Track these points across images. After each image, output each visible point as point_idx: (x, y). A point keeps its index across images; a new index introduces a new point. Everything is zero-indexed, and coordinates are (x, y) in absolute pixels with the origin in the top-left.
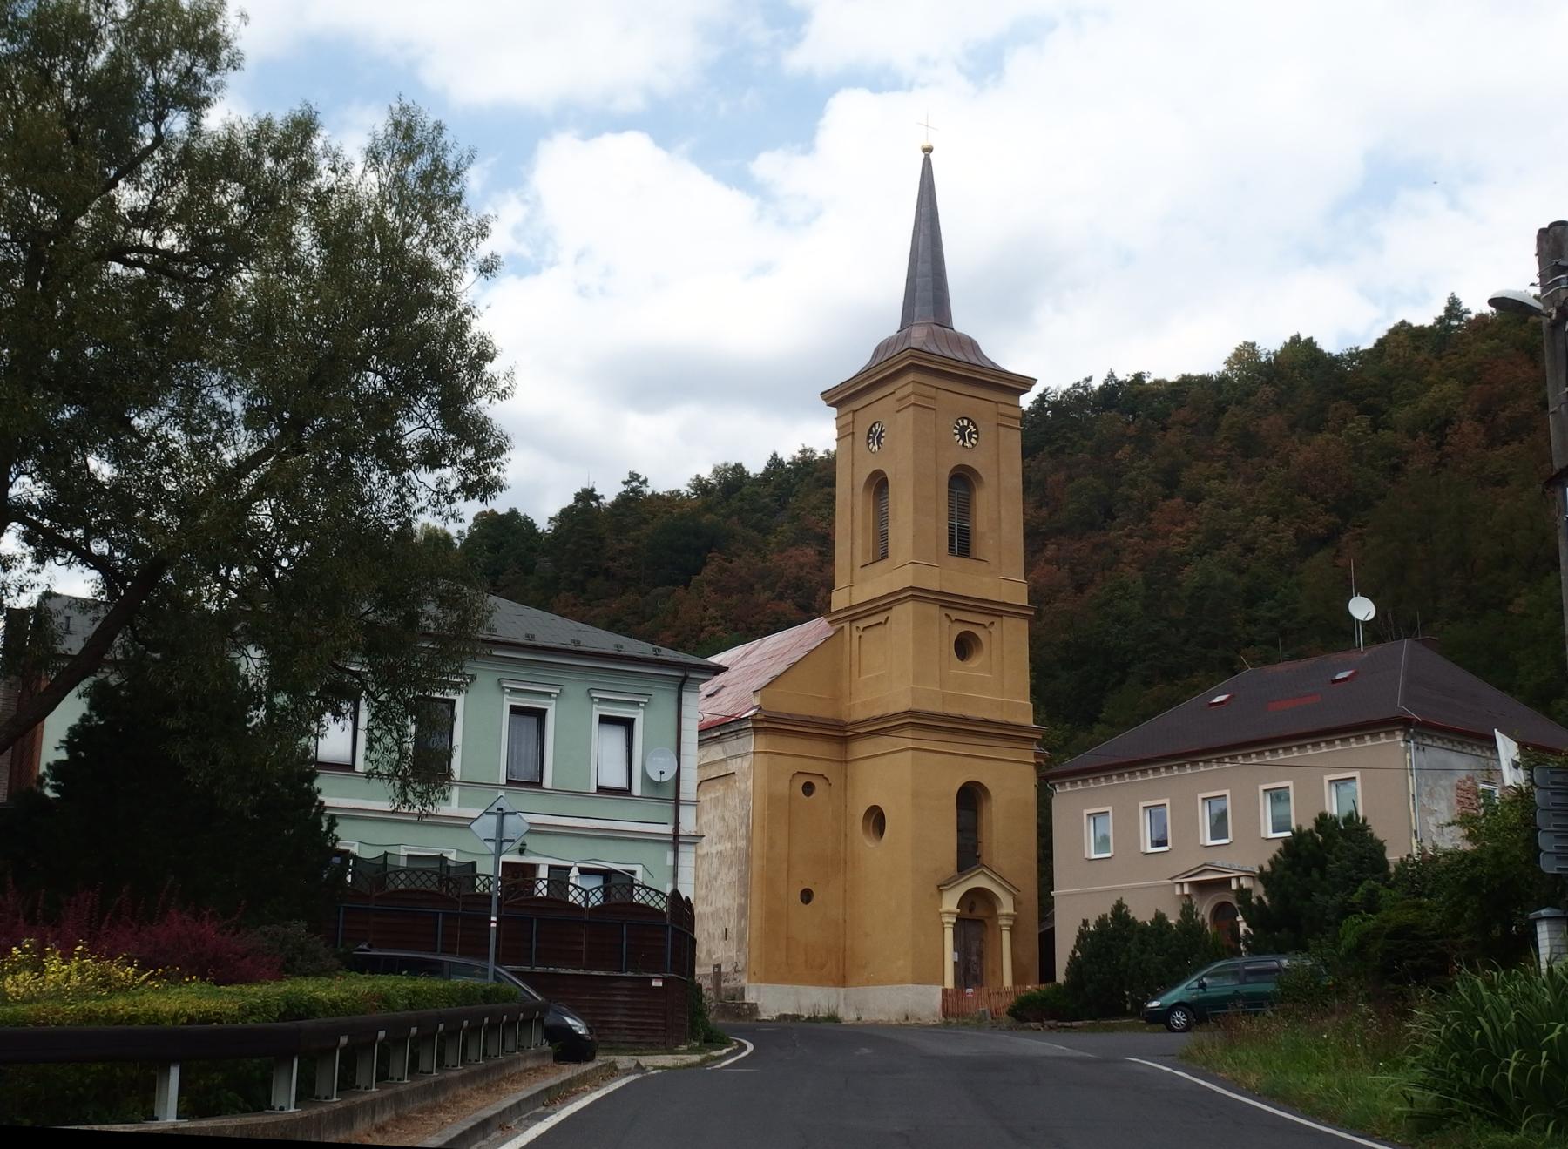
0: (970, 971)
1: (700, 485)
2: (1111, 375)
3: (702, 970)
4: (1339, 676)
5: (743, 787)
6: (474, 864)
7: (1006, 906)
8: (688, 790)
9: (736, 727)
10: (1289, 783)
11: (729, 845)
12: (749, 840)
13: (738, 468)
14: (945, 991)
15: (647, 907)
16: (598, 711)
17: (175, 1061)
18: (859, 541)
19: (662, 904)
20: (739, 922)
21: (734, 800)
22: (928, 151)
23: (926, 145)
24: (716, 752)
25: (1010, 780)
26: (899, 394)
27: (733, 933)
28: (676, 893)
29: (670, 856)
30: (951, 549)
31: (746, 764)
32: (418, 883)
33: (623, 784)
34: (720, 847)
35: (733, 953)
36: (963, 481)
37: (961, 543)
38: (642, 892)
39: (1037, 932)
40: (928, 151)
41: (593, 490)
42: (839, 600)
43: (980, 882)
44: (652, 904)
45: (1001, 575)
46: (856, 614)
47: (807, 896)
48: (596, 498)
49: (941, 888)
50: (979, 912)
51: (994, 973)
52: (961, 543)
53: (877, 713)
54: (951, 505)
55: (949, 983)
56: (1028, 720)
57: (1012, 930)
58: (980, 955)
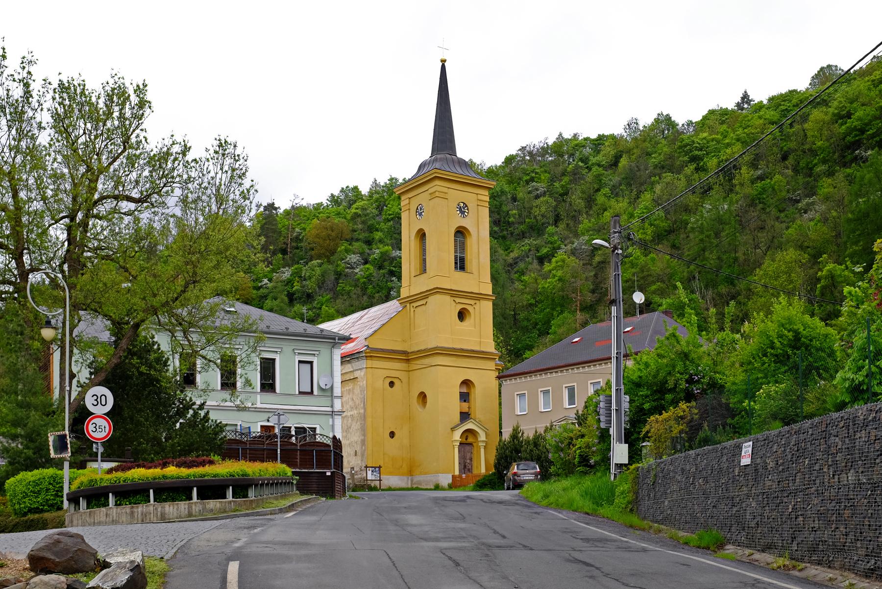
0: (465, 466)
1: (334, 199)
2: (560, 135)
3: (346, 470)
7: (482, 437)
8: (337, 391)
9: (357, 356)
10: (575, 384)
13: (356, 188)
14: (453, 476)
21: (357, 391)
22: (443, 61)
23: (444, 58)
24: (348, 368)
25: (485, 378)
26: (431, 191)
27: (359, 453)
28: (334, 437)
29: (331, 420)
30: (456, 268)
31: (362, 374)
34: (352, 413)
35: (359, 462)
36: (461, 233)
37: (461, 264)
40: (443, 61)
41: (273, 204)
42: (404, 293)
43: (469, 425)
45: (479, 278)
46: (412, 300)
47: (392, 435)
48: (276, 209)
49: (453, 429)
50: (470, 440)
52: (461, 264)
53: (423, 348)
54: (455, 246)
55: (457, 473)
56: (493, 350)
58: (471, 459)
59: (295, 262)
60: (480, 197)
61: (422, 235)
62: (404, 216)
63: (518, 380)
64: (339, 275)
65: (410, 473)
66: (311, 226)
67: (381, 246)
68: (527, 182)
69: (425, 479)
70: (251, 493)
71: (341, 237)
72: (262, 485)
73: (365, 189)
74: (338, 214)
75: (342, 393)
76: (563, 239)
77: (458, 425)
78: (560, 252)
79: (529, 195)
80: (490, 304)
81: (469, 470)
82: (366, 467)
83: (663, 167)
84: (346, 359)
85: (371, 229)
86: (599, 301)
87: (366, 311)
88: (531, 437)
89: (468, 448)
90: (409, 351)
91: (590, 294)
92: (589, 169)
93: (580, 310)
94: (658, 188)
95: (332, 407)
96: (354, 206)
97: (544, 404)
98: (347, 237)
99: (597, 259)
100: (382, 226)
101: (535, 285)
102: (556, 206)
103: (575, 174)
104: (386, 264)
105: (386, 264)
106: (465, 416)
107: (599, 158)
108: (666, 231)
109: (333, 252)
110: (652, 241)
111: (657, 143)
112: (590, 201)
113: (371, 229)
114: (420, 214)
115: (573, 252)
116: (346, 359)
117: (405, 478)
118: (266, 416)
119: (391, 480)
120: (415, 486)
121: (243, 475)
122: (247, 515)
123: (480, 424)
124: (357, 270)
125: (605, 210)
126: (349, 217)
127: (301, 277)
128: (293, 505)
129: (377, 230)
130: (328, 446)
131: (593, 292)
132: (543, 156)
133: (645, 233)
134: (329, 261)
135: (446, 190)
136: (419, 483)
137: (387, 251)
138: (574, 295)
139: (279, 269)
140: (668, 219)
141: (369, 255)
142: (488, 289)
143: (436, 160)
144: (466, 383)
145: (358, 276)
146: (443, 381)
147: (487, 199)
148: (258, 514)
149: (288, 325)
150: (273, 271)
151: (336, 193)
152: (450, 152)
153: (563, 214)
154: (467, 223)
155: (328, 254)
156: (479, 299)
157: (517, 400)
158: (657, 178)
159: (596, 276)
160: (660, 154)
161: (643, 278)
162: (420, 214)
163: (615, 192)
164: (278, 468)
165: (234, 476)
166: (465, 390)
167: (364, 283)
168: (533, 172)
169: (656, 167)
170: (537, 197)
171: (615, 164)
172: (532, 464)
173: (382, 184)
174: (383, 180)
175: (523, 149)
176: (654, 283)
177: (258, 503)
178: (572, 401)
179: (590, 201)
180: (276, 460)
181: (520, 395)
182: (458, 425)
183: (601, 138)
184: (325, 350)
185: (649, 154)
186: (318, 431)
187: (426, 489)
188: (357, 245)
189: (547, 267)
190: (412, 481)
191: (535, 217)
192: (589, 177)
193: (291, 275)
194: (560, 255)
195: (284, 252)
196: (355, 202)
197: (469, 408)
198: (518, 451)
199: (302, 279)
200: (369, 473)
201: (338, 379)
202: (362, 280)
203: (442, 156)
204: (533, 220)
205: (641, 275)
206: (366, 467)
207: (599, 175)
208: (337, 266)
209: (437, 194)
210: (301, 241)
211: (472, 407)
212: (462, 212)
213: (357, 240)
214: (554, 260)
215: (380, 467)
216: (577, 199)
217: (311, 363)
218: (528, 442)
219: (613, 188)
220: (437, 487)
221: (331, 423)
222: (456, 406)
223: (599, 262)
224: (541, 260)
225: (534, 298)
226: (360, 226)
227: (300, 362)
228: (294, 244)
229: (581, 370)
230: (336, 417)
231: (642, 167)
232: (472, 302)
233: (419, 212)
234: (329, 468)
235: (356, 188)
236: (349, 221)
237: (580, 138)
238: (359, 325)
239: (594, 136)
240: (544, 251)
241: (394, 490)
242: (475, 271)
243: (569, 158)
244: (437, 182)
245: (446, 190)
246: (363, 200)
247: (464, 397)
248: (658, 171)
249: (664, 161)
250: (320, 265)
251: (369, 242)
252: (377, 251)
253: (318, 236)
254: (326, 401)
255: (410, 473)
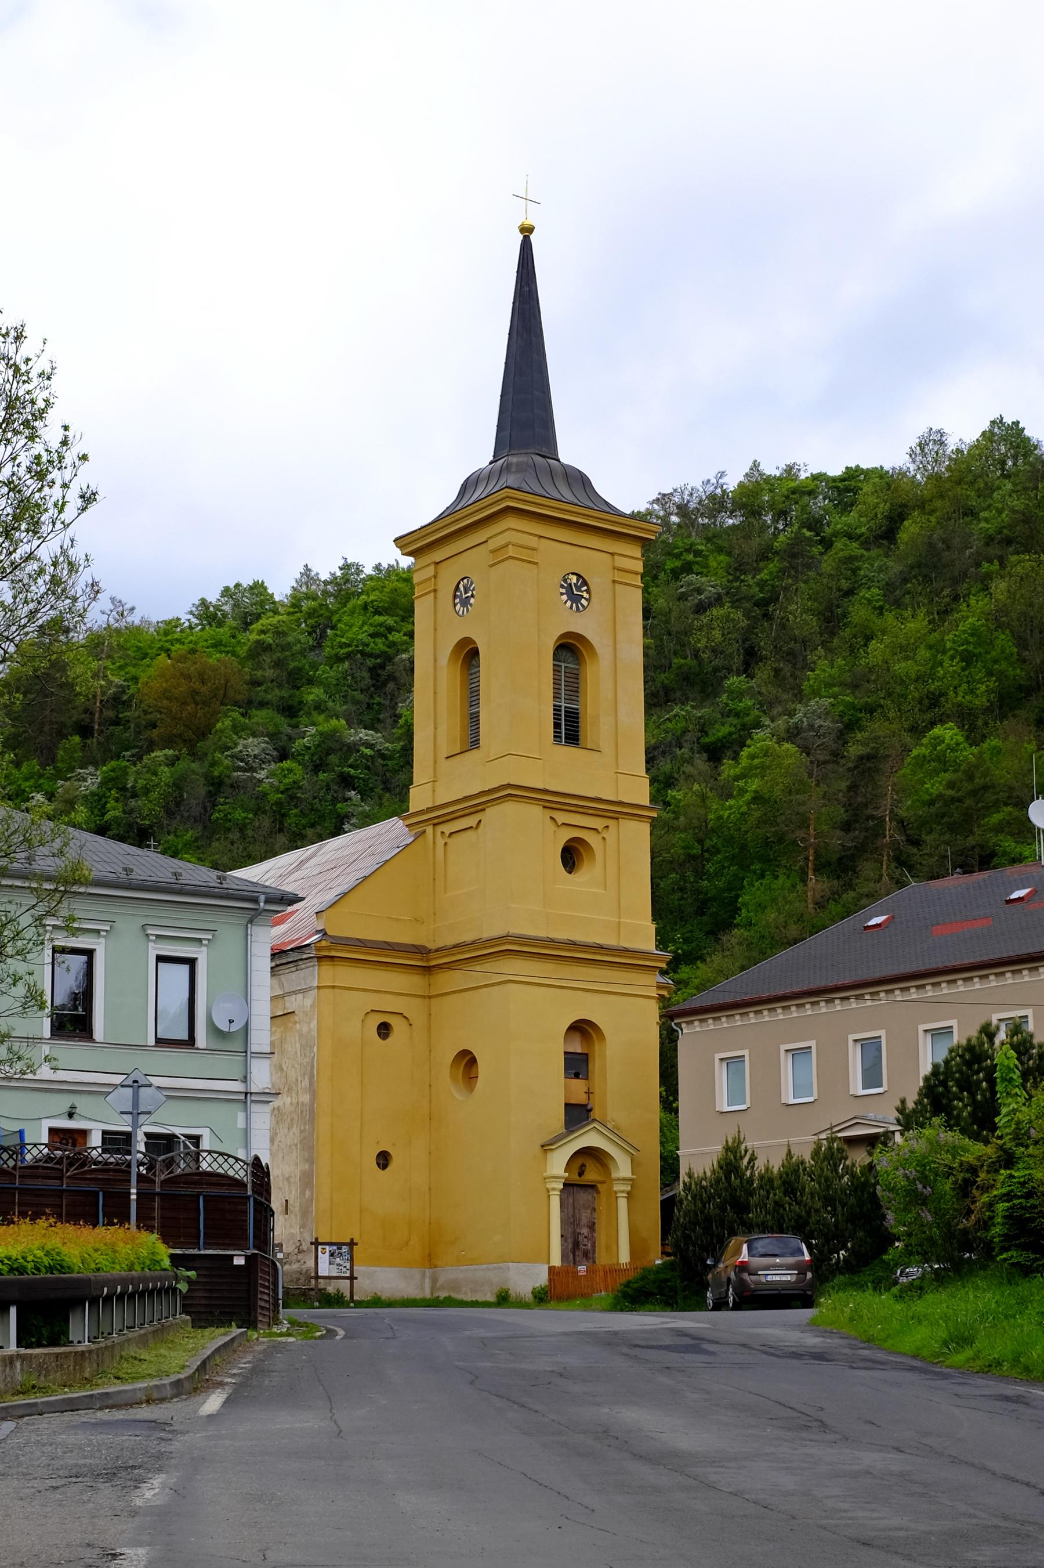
0: (578, 1244)
1: (207, 614)
2: (755, 465)
4: (1015, 895)
5: (305, 1029)
6: (21, 1133)
7: (623, 1168)
8: (261, 1038)
11: (288, 1100)
12: (313, 1091)
13: (258, 588)
14: (551, 1269)
15: (225, 1176)
16: (155, 950)
17: (13, 1304)
18: (443, 728)
19: (242, 1173)
20: (303, 1193)
22: (527, 231)
23: (529, 222)
26: (493, 544)
29: (241, 1116)
30: (557, 737)
31: (308, 1002)
32: (226, 1166)
33: (184, 1036)
35: (296, 1230)
36: (570, 650)
37: (569, 728)
38: (209, 1159)
39: (659, 1198)
40: (527, 231)
42: (419, 798)
43: (589, 1138)
44: (231, 1173)
45: (617, 760)
46: (440, 816)
47: (384, 1159)
49: (547, 1147)
50: (591, 1175)
51: (608, 1248)
52: (569, 728)
53: (468, 938)
54: (556, 682)
55: (556, 1261)
57: (630, 1196)
58: (592, 1227)
59: (109, 754)
60: (621, 562)
61: (469, 655)
62: (422, 609)
63: (724, 1023)
64: (217, 786)
65: (430, 1260)
66: (151, 671)
67: (321, 718)
68: (676, 574)
69: (477, 1279)
70: (80, 1330)
71: (223, 696)
72: (108, 1299)
73: (281, 589)
74: (217, 645)
75: (272, 1044)
76: (766, 706)
77: (559, 1138)
78: (759, 734)
79: (682, 605)
80: (645, 828)
81: (586, 1254)
82: (316, 1243)
83: (1009, 541)
84: (283, 958)
85: (297, 679)
86: (862, 849)
87: (313, 848)
88: (776, 1166)
89: (583, 1196)
90: (431, 946)
91: (839, 833)
92: (827, 544)
93: (816, 870)
94: (1000, 587)
95: (245, 1080)
96: (257, 626)
97: (810, 1077)
98: (240, 697)
99: (854, 750)
100: (324, 671)
101: (702, 811)
102: (750, 629)
103: (794, 556)
104: (333, 759)
105: (333, 759)
106: (577, 1115)
107: (852, 518)
108: (1020, 688)
109: (204, 732)
110: (988, 710)
111: (991, 489)
112: (832, 619)
113: (297, 679)
114: (465, 603)
115: (793, 734)
116: (283, 958)
117: (416, 1273)
118: (64, 1103)
119: (379, 1279)
120: (443, 1295)
121: (50, 1269)
122: (71, 1406)
123: (616, 1134)
124: (261, 775)
125: (868, 638)
126: (242, 651)
127: (124, 789)
128: (204, 1363)
129: (310, 682)
130: (240, 1184)
131: (847, 827)
132: (713, 514)
133: (972, 691)
134: (193, 754)
135: (533, 542)
136: (455, 1285)
137: (335, 731)
138: (800, 833)
139: (72, 769)
140: (1024, 661)
141: (291, 739)
142: (640, 791)
143: (506, 469)
144: (582, 1029)
145: (265, 786)
146: (522, 1022)
147: (639, 567)
148: (108, 1402)
149: (130, 862)
150: (59, 775)
151: (213, 596)
152: (544, 451)
153: (764, 644)
154: (584, 624)
155: (192, 737)
156: (616, 816)
157: (787, 1064)
158: (996, 566)
159: (853, 788)
160: (1000, 512)
161: (974, 793)
162: (465, 603)
163: (894, 597)
164: (128, 1248)
165: (21, 1270)
166: (577, 1047)
167: (279, 803)
168: (688, 551)
169: (989, 540)
170: (701, 608)
171: (887, 533)
172: (795, 1241)
173: (325, 576)
174: (326, 569)
175: (663, 499)
176: (996, 806)
177: (97, 1362)
178: (872, 1077)
179: (832, 619)
180: (128, 1219)
181: (794, 1052)
182: (559, 1138)
183: (852, 474)
184: (228, 930)
185: (971, 513)
186: (205, 1144)
187: (474, 1304)
188: (260, 716)
189: (728, 769)
190: (434, 1280)
191: (696, 656)
192: (828, 564)
193: (101, 785)
194: (761, 740)
195: (85, 731)
196: (258, 617)
197: (589, 1093)
198: (741, 1208)
199: (128, 793)
200: (324, 1259)
201: (261, 1010)
202: (274, 797)
203: (523, 459)
204: (690, 662)
205: (968, 786)
206: (316, 1243)
207: (851, 559)
208: (214, 764)
209: (511, 551)
210: (127, 704)
211: (597, 1090)
212: (575, 599)
213: (262, 705)
214: (745, 753)
215: (352, 1244)
216: (799, 613)
217: (191, 962)
218: (767, 1180)
219: (889, 588)
220: (503, 1299)
221: (241, 1124)
222: (555, 1089)
223: (861, 758)
224: (715, 753)
225: (700, 842)
226: (270, 673)
227: (160, 959)
228: (110, 714)
229: (914, 994)
230: (255, 1108)
231: (957, 541)
232: (597, 823)
233: (462, 595)
234: (240, 1244)
235: (258, 588)
236: (243, 661)
237: (803, 476)
238: (315, 874)
239: (836, 471)
240: (721, 731)
241: (390, 1304)
242: (605, 744)
243: (775, 520)
244: (512, 522)
245: (533, 542)
246: (276, 612)
247: (577, 1066)
248: (994, 550)
249: (1010, 527)
250: (172, 762)
251: (291, 710)
252: (312, 730)
253: (166, 694)
254: (231, 1065)
255: (430, 1260)
